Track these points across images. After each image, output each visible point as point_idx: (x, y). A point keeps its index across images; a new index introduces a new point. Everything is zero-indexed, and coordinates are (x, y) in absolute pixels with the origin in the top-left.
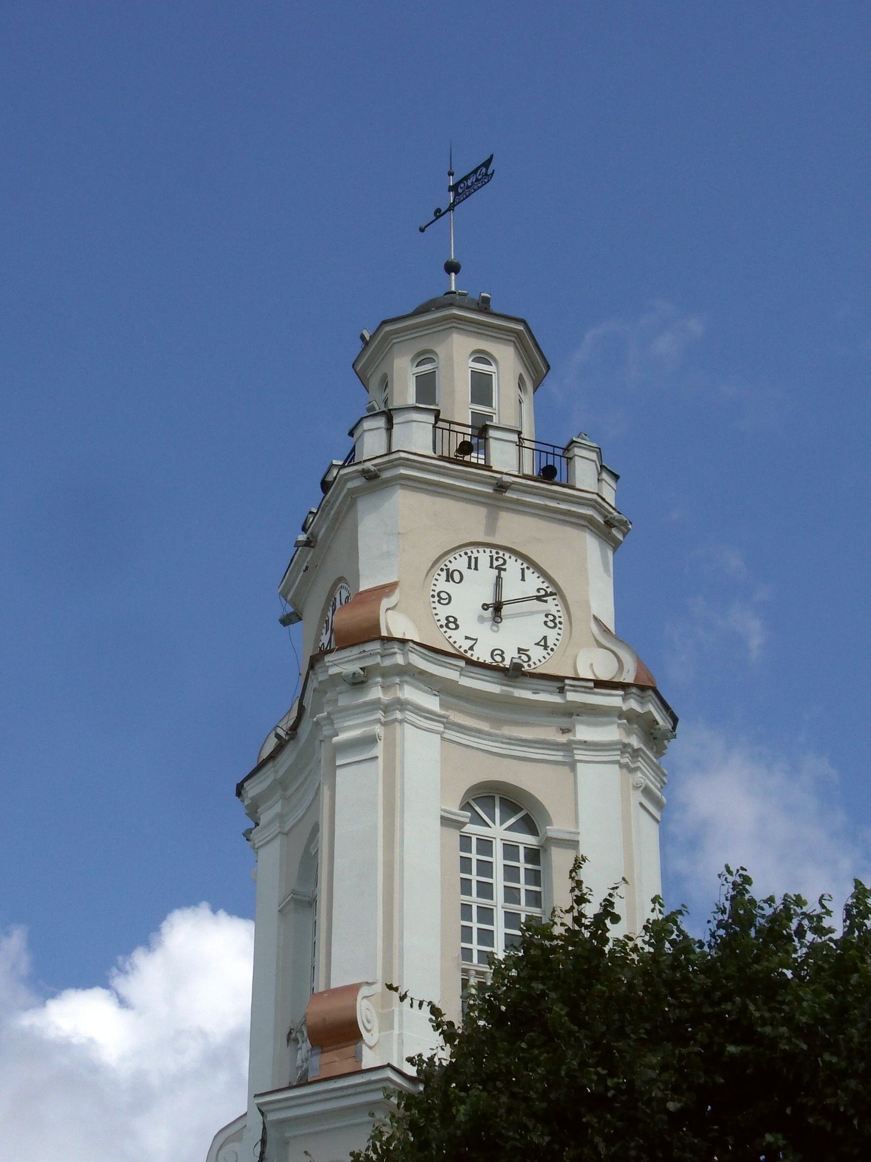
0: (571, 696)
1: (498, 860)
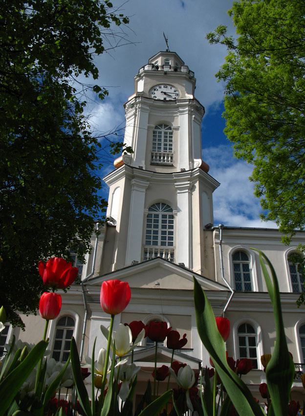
0: (178, 103)
1: (160, 219)
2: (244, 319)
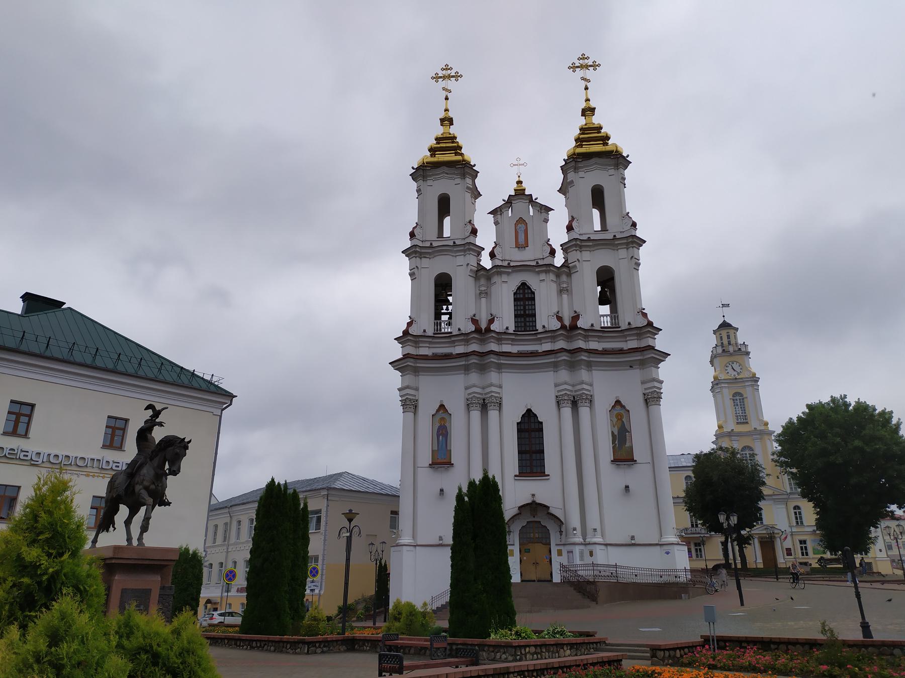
2: (803, 538)
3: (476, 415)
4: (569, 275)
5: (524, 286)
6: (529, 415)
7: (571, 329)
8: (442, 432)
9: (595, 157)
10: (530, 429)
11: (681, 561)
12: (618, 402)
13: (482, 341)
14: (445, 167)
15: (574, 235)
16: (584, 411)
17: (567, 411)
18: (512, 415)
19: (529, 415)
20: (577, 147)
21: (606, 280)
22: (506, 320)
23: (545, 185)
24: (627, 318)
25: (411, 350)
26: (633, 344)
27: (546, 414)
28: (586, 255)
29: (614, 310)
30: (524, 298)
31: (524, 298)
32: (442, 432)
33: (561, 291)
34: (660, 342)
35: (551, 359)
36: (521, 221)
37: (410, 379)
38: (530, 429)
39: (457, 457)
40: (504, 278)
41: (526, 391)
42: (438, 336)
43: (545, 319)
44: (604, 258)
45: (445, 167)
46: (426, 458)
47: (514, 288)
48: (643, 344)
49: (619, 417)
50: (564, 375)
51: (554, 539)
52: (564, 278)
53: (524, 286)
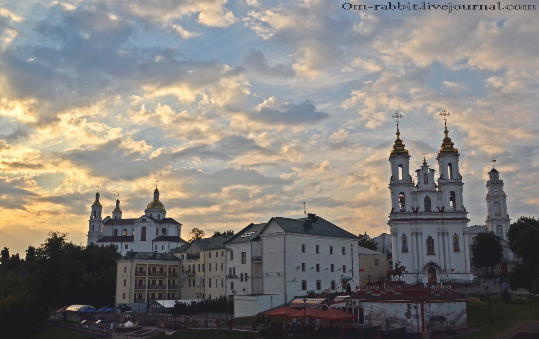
3: (414, 237)
4: (441, 193)
5: (427, 196)
6: (430, 237)
7: (442, 211)
8: (405, 242)
9: (448, 152)
10: (430, 241)
11: (471, 277)
12: (455, 234)
13: (416, 215)
14: (399, 153)
15: (442, 181)
16: (446, 237)
17: (441, 237)
18: (425, 238)
19: (430, 237)
20: (109, 130)
21: (453, 197)
22: (422, 209)
23: (431, 158)
24: (458, 208)
25: (393, 218)
26: (460, 217)
27: (435, 237)
28: (446, 187)
29: (454, 204)
30: (427, 201)
31: (427, 201)
32: (405, 242)
33: (438, 199)
34: (468, 217)
35: (437, 221)
36: (426, 174)
37: (394, 227)
38: (430, 241)
39: (409, 249)
40: (421, 195)
41: (429, 230)
42: (403, 211)
43: (434, 208)
44: (452, 188)
45: (399, 153)
46: (400, 249)
47: (424, 198)
48: (463, 217)
49: (456, 238)
50: (440, 226)
51: (437, 272)
52: (440, 194)
53: (427, 196)
